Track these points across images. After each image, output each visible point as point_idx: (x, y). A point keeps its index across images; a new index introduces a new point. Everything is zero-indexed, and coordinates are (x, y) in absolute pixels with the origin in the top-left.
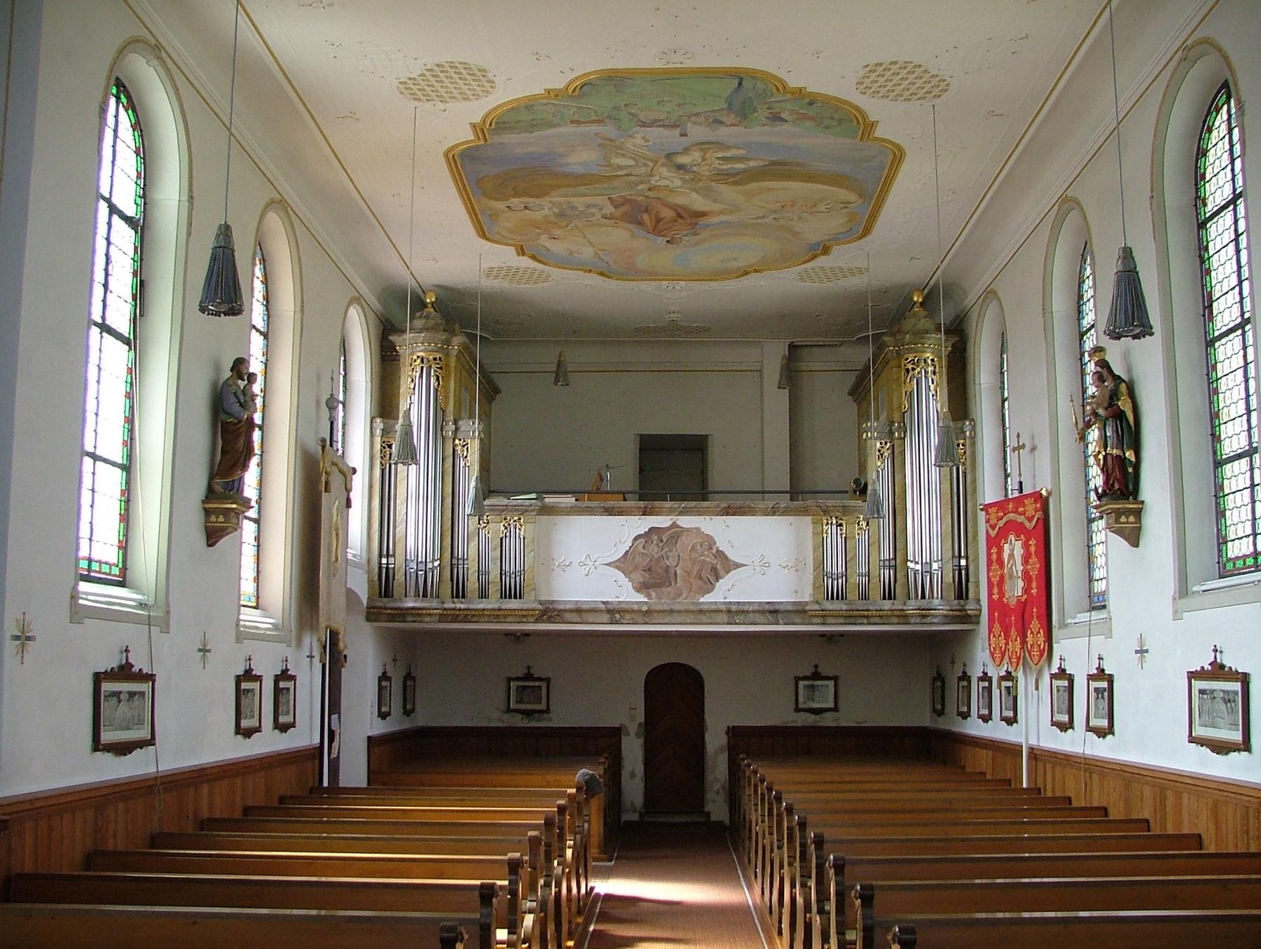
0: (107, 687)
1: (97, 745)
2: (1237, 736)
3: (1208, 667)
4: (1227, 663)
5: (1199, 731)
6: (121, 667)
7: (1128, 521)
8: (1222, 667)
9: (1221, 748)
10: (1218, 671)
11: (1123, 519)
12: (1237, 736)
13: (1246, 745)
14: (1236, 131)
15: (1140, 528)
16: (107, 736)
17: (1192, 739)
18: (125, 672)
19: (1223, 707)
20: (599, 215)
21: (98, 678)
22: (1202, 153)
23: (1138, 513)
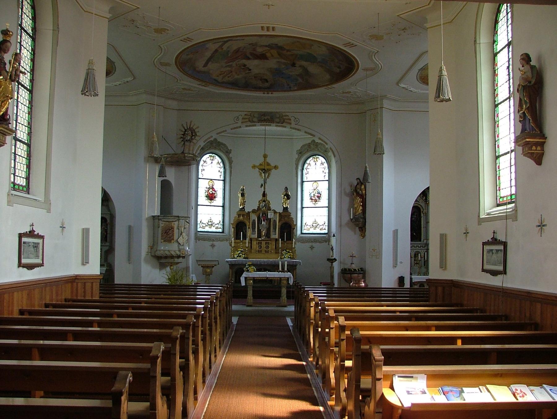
0: (24, 239)
1: (20, 265)
2: (501, 268)
3: (490, 240)
4: (498, 238)
5: (486, 267)
6: (30, 232)
7: (536, 150)
8: (496, 239)
9: (494, 273)
10: (495, 241)
11: (534, 148)
12: (501, 268)
13: (504, 272)
14: (509, 15)
15: (543, 154)
16: (24, 261)
17: (483, 270)
18: (31, 234)
19: (32, 249)
20: (253, 236)
21: (21, 236)
22: (496, 22)
23: (542, 144)
